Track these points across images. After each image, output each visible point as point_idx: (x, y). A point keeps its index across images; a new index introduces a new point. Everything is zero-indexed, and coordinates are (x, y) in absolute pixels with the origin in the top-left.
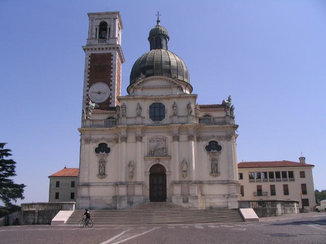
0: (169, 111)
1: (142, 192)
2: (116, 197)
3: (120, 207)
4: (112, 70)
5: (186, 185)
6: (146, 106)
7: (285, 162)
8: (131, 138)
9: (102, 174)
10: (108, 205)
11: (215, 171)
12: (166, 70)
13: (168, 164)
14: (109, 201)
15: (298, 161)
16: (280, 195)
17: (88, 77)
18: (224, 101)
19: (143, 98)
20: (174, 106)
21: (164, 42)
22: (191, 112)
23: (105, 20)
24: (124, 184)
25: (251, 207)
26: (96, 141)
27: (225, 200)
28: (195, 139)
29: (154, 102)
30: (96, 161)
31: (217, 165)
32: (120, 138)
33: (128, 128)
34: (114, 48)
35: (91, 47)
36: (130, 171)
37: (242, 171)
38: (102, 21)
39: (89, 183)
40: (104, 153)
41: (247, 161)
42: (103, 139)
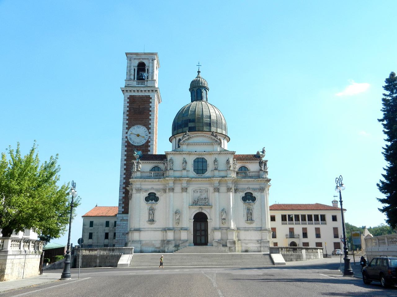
1: (187, 236)
2: (164, 241)
3: (167, 250)
4: (150, 113)
5: (225, 231)
6: (191, 160)
7: (317, 204)
8: (178, 188)
9: (152, 221)
11: (250, 218)
13: (209, 212)
14: (158, 245)
15: (331, 205)
16: (312, 239)
18: (258, 153)
19: (188, 154)
20: (215, 161)
21: (204, 94)
22: (230, 167)
24: (171, 230)
25: (280, 253)
26: (146, 191)
27: (258, 245)
28: (233, 191)
29: (198, 157)
30: (147, 209)
31: (251, 214)
32: (167, 189)
33: (177, 179)
34: (152, 91)
35: (130, 89)
36: (177, 218)
37: (274, 213)
38: (140, 61)
39: (140, 228)
40: (153, 201)
41: (279, 203)
42: (153, 188)
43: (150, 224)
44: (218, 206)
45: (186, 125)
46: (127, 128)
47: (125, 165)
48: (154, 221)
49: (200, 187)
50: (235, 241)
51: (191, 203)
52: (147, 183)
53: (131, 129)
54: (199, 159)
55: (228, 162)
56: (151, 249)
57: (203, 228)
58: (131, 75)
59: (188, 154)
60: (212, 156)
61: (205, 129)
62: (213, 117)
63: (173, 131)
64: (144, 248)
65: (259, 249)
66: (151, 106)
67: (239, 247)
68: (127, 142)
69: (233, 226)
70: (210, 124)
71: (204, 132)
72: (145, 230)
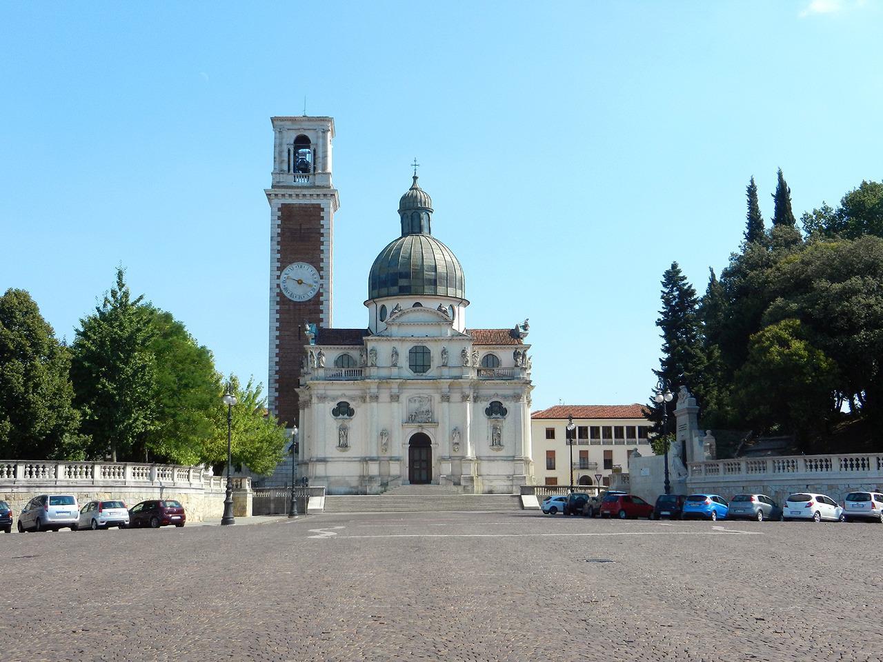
0: (436, 360)
1: (399, 469)
2: (364, 476)
3: (370, 490)
6: (404, 350)
8: (385, 395)
9: (344, 446)
10: (352, 487)
11: (497, 442)
12: (430, 280)
17: (279, 252)
19: (400, 340)
20: (444, 352)
21: (424, 222)
23: (306, 133)
26: (334, 399)
27: (509, 483)
28: (472, 399)
29: (416, 344)
30: (335, 428)
31: (499, 436)
32: (368, 397)
37: (550, 424)
38: (299, 134)
39: (325, 458)
43: (341, 451)
44: (447, 424)
45: (395, 283)
46: (279, 269)
47: (277, 337)
48: (347, 446)
49: (420, 394)
50: (473, 477)
51: (405, 418)
52: (334, 387)
53: (286, 271)
54: (418, 348)
55: (464, 353)
56: (343, 489)
57: (424, 457)
58: (282, 162)
59: (400, 340)
60: (439, 343)
61: (428, 290)
62: (441, 269)
63: (371, 289)
64: (334, 488)
65: (510, 488)
66: (323, 225)
67: (479, 487)
68: (280, 294)
69: (470, 454)
70: (435, 281)
71: (425, 296)
72: (334, 460)
